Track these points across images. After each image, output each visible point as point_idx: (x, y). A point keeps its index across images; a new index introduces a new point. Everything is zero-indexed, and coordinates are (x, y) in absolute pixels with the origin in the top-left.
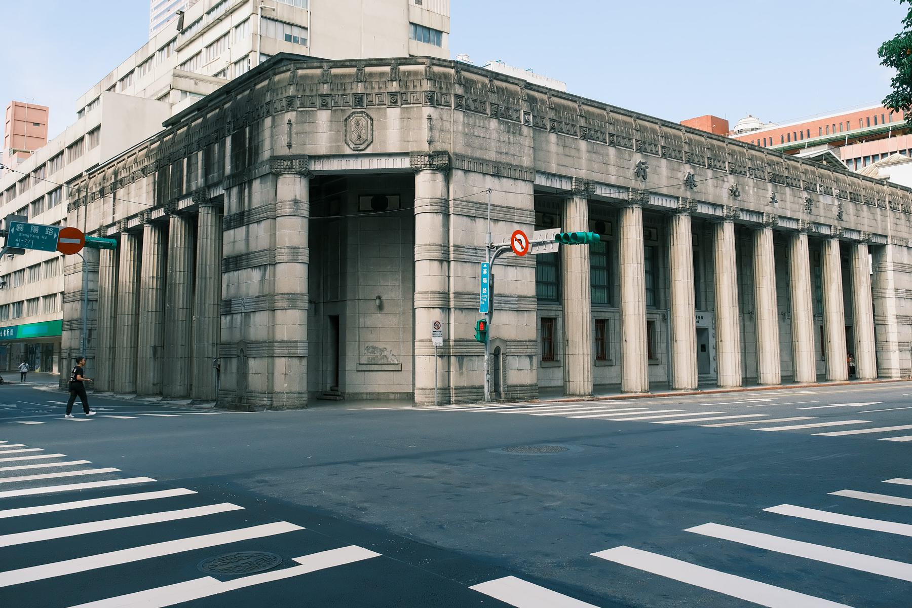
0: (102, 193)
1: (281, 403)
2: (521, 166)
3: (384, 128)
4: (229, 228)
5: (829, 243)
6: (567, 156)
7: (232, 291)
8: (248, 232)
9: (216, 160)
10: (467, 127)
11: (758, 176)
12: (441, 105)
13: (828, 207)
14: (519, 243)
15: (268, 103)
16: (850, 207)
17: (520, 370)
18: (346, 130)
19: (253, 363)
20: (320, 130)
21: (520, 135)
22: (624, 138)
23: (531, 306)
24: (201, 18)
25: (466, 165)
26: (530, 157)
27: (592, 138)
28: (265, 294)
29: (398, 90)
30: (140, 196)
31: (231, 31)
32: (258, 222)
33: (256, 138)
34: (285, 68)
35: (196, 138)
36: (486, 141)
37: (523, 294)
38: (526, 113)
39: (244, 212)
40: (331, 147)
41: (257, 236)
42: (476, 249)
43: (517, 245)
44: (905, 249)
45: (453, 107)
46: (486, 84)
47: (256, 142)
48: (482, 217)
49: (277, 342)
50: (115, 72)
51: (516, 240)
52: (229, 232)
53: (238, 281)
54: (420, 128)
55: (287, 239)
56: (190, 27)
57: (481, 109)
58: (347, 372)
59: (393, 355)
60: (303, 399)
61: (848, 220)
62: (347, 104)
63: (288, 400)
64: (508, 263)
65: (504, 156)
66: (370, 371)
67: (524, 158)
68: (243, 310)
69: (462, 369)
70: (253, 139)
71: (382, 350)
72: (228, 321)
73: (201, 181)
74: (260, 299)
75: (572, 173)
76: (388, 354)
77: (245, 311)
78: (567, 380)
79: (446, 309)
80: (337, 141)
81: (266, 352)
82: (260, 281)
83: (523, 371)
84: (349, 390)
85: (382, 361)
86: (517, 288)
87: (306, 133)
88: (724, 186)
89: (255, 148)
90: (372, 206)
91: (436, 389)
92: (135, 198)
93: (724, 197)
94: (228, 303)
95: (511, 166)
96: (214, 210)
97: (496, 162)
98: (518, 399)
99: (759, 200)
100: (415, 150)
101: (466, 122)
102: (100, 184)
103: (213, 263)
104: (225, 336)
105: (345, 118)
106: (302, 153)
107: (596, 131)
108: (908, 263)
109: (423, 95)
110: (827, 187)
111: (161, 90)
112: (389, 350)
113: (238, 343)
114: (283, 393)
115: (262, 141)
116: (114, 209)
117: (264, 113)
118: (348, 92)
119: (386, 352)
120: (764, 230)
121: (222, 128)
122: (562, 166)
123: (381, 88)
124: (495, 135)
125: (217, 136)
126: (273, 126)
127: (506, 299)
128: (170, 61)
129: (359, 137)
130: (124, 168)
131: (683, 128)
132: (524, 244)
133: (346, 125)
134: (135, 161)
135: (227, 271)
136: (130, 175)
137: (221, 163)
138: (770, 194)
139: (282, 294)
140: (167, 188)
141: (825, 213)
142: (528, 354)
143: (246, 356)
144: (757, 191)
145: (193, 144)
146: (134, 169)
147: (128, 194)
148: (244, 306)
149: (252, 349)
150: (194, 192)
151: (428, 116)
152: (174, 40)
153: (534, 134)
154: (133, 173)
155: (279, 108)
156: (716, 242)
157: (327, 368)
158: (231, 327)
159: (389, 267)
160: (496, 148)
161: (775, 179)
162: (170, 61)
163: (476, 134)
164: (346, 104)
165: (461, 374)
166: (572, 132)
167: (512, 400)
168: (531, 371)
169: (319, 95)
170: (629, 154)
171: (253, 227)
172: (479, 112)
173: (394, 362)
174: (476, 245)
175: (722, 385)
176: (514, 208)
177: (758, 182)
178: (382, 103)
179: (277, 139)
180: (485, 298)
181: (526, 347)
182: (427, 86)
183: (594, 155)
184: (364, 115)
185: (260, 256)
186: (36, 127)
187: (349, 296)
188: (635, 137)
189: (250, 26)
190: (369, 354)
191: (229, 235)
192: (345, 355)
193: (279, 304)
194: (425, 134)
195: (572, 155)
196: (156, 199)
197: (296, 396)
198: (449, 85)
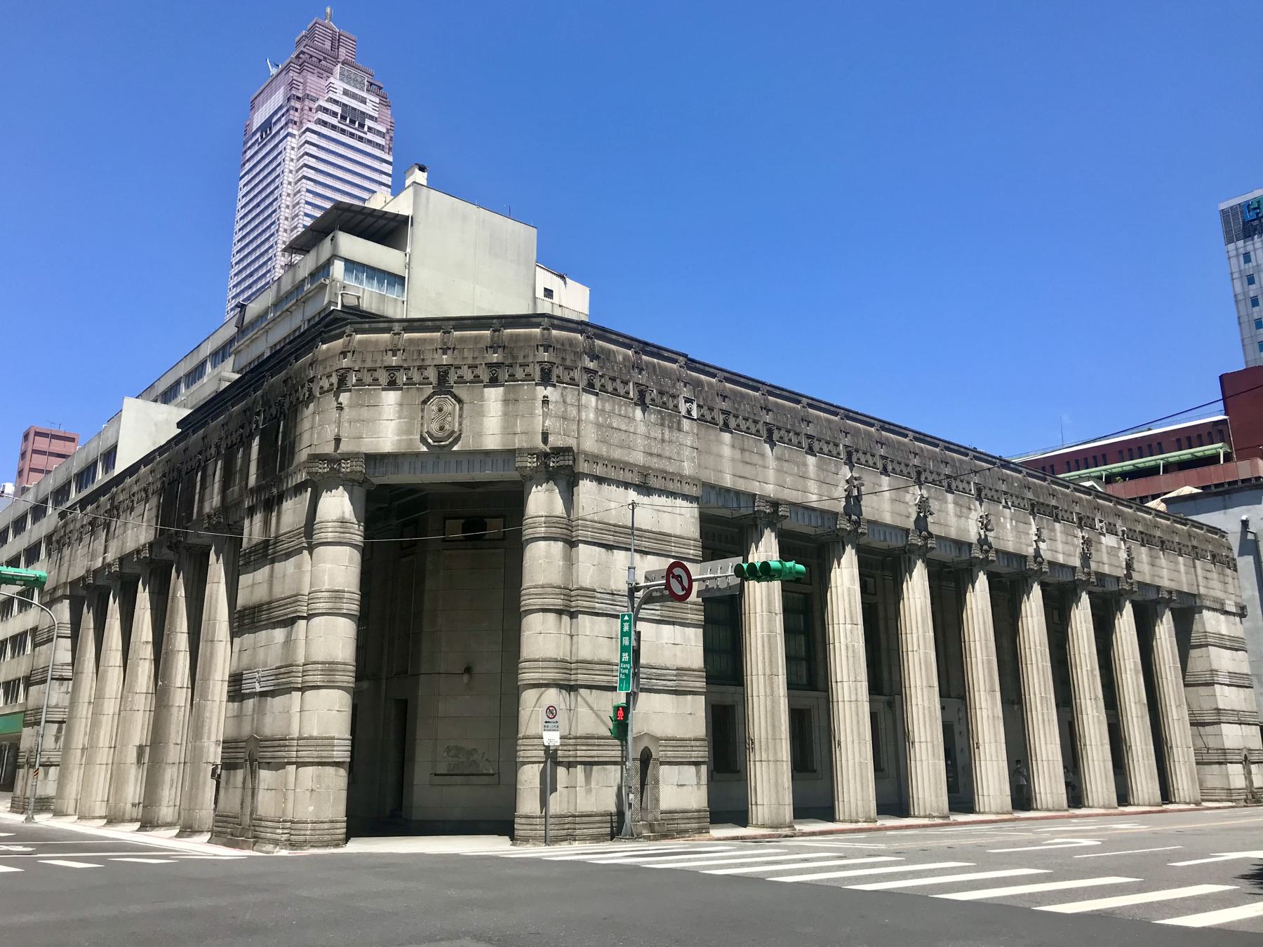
2: (681, 476)
6: (747, 463)
8: (272, 571)
9: (238, 468)
10: (601, 415)
11: (1016, 504)
12: (563, 383)
13: (1113, 551)
15: (311, 380)
16: (1143, 554)
17: (681, 785)
20: (385, 417)
21: (679, 429)
22: (828, 443)
25: (599, 470)
29: (501, 360)
33: (293, 430)
36: (629, 437)
37: (685, 665)
40: (400, 441)
41: (284, 575)
42: (613, 594)
43: (675, 585)
46: (629, 356)
54: (532, 414)
55: (326, 578)
57: (622, 391)
58: (415, 787)
59: (487, 760)
60: (338, 831)
61: (1141, 570)
62: (426, 381)
63: (313, 832)
64: (661, 616)
65: (655, 460)
67: (685, 464)
69: (590, 784)
71: (471, 752)
73: (216, 500)
75: (755, 488)
80: (409, 431)
83: (685, 787)
86: (675, 655)
87: (364, 421)
88: (970, 516)
93: (972, 531)
94: (238, 677)
95: (666, 475)
97: (644, 467)
98: (678, 833)
99: (1020, 538)
100: (525, 445)
101: (600, 407)
105: (422, 399)
106: (356, 450)
107: (788, 432)
108: (1227, 634)
109: (538, 369)
110: (1110, 524)
114: (306, 822)
115: (300, 434)
117: (304, 395)
118: (427, 363)
122: (740, 477)
123: (477, 357)
124: (642, 429)
127: (659, 671)
129: (442, 428)
131: (911, 433)
132: (686, 584)
137: (245, 471)
138: (1034, 530)
141: (1109, 558)
144: (1016, 525)
153: (698, 429)
155: (326, 386)
160: (644, 447)
161: (1036, 509)
163: (615, 425)
166: (753, 430)
167: (670, 835)
168: (699, 789)
169: (385, 367)
172: (620, 396)
174: (613, 588)
176: (670, 535)
177: (1017, 513)
178: (477, 379)
180: (626, 668)
181: (690, 749)
183: (786, 464)
186: (21, 437)
187: (424, 668)
188: (843, 441)
192: (412, 759)
195: (755, 462)
197: (326, 826)
198: (578, 355)
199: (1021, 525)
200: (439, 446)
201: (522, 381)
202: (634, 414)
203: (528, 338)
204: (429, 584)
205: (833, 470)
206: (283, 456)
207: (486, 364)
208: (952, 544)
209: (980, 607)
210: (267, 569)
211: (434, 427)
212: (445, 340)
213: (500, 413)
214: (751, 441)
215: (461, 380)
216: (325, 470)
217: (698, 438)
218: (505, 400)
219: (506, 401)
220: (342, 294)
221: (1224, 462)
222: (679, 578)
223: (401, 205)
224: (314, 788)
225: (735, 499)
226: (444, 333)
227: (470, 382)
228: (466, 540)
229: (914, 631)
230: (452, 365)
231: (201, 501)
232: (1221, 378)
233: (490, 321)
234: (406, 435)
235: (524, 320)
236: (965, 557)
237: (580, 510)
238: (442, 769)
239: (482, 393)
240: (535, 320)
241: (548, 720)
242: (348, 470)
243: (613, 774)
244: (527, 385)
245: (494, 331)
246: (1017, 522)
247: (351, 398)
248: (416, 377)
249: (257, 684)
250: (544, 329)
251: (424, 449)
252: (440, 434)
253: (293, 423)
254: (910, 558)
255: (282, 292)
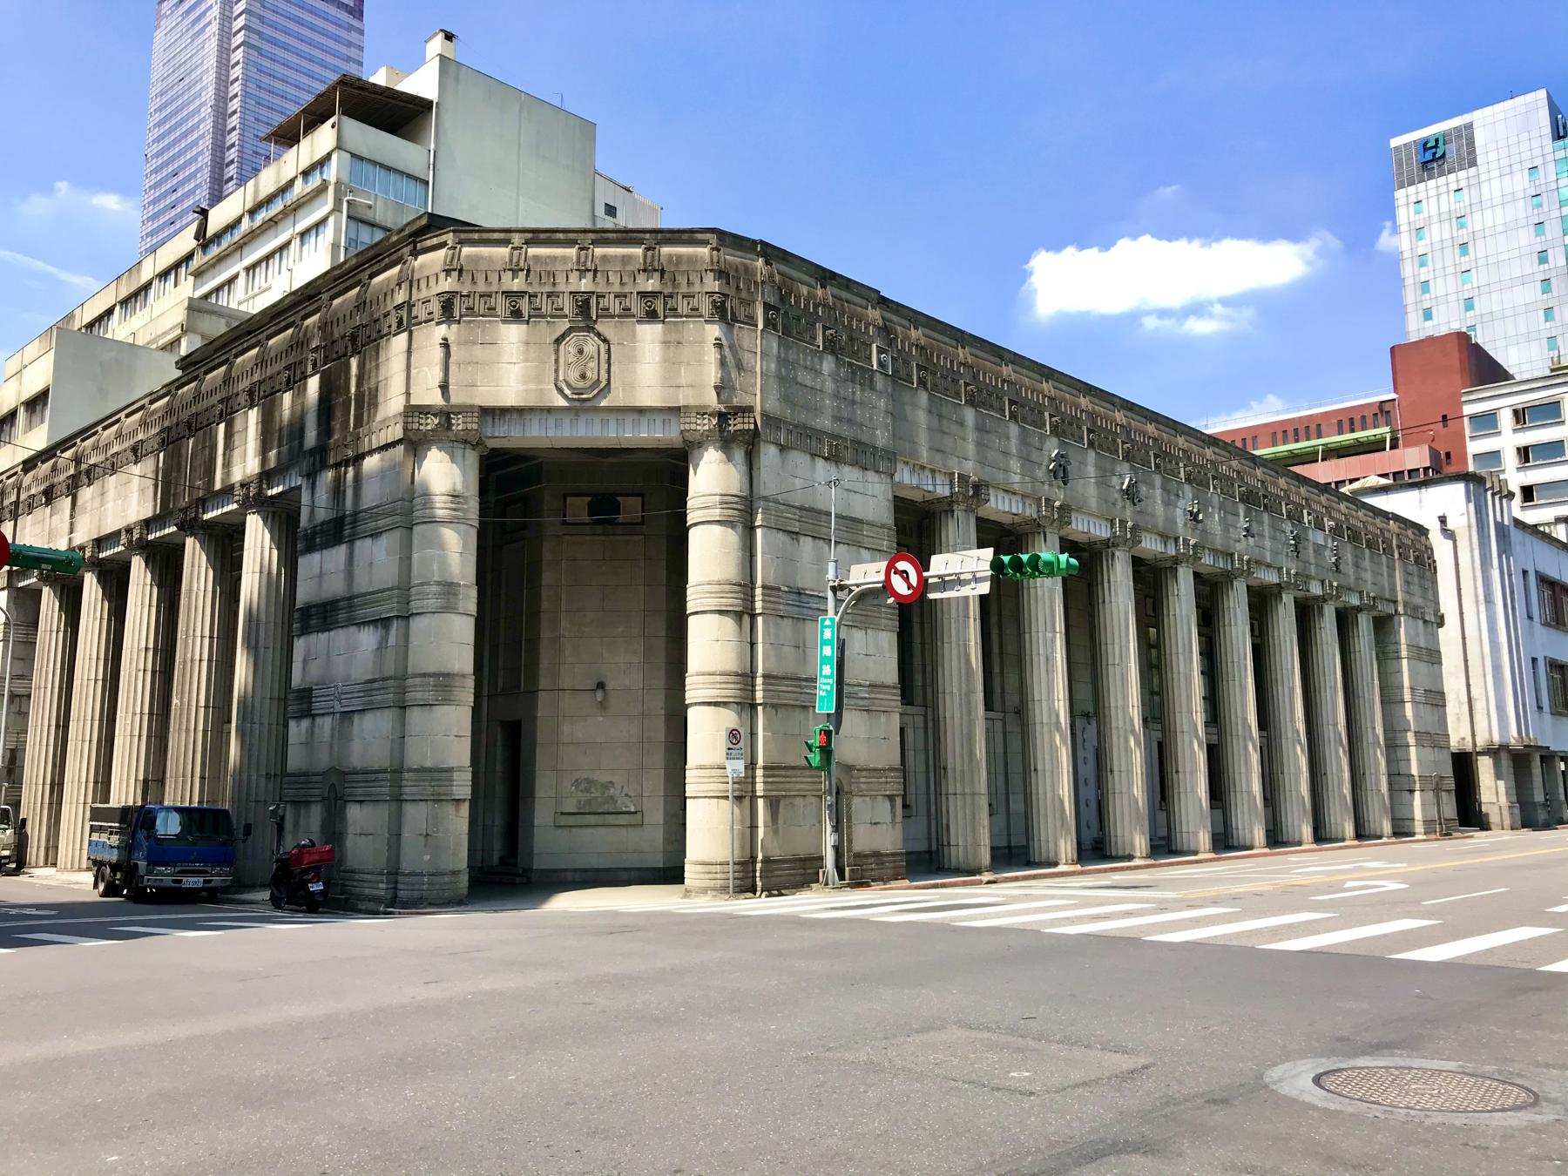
0: (49, 495)
1: (416, 894)
3: (633, 359)
4: (310, 549)
5: (1321, 609)
7: (315, 672)
14: (903, 577)
17: (876, 824)
18: (557, 361)
19: (355, 813)
20: (506, 358)
21: (872, 388)
23: (893, 703)
24: (239, 221)
26: (888, 431)
27: (983, 404)
28: (386, 675)
29: (657, 289)
30: (126, 496)
31: (293, 242)
32: (375, 535)
33: (373, 374)
34: (435, 241)
35: (245, 384)
38: (880, 351)
39: (344, 517)
44: (1420, 623)
45: (761, 326)
47: (373, 381)
48: (810, 533)
49: (411, 770)
50: (78, 312)
51: (895, 573)
52: (309, 556)
53: (328, 651)
54: (700, 361)
56: (218, 236)
59: (626, 795)
66: (581, 826)
67: (878, 432)
68: (338, 708)
70: (366, 377)
72: (303, 731)
74: (375, 685)
76: (617, 793)
77: (342, 710)
78: (945, 843)
79: (747, 706)
80: (539, 380)
81: (386, 790)
82: (377, 649)
84: (538, 864)
85: (606, 808)
86: (867, 668)
89: (370, 393)
90: (619, 503)
91: (731, 863)
92: (115, 501)
96: (277, 518)
99: (1228, 531)
100: (691, 402)
102: (46, 478)
103: (272, 619)
104: (295, 761)
105: (555, 336)
106: (469, 401)
111: (165, 334)
112: (618, 786)
113: (323, 774)
114: (421, 874)
115: (386, 379)
116: (72, 524)
117: (390, 326)
118: (560, 288)
119: (612, 790)
120: (1235, 583)
121: (301, 363)
123: (625, 284)
124: (829, 386)
125: (289, 376)
126: (229, 436)
128: (187, 288)
129: (583, 376)
130: (95, 448)
133: (557, 352)
134: (119, 435)
135: (305, 631)
136: (107, 459)
139: (424, 675)
140: (183, 476)
141: (1315, 557)
142: (888, 793)
143: (341, 798)
145: (237, 395)
146: (116, 449)
147: (102, 494)
148: (340, 700)
149: (354, 785)
150: (237, 485)
151: (716, 339)
152: (189, 257)
154: (113, 456)
155: (423, 316)
156: (1165, 600)
157: (493, 822)
158: (310, 741)
159: (620, 630)
162: (187, 288)
164: (559, 313)
165: (776, 832)
168: (893, 827)
170: (1040, 439)
171: (363, 546)
173: (627, 809)
174: (800, 586)
175: (1179, 848)
177: (1226, 502)
178: (626, 313)
179: (418, 373)
180: (828, 684)
182: (711, 284)
184: (592, 335)
185: (377, 602)
187: (544, 682)
189: (328, 234)
190: (579, 794)
191: (309, 564)
192: (532, 795)
193: (413, 696)
194: (712, 374)
196: (159, 501)
199: (1230, 517)
200: (578, 400)
201: (686, 316)
202: (821, 366)
203: (692, 260)
204: (547, 577)
205: (1037, 445)
206: (359, 406)
207: (638, 293)
208: (1157, 537)
209: (1184, 612)
210: (342, 550)
211: (573, 376)
212: (582, 260)
213: (657, 359)
214: (950, 405)
215: (606, 313)
216: (706, 428)
217: (893, 400)
218: (665, 342)
219: (666, 343)
220: (348, 201)
221: (1391, 448)
222: (904, 575)
223: (422, 83)
224: (429, 832)
225: (930, 477)
226: (581, 249)
227: (619, 316)
228: (593, 524)
229: (1116, 641)
230: (593, 293)
231: (227, 465)
232: (1392, 349)
233: (642, 235)
234: (525, 383)
235: (686, 236)
236: (1171, 551)
237: (762, 488)
238: (570, 806)
239: (634, 332)
240: (699, 236)
241: (732, 746)
242: (460, 428)
243: (802, 809)
244: (694, 322)
245: (581, 249)
246: (1225, 513)
247: (459, 330)
248: (546, 307)
249: (336, 703)
250: (713, 249)
251: (565, 404)
252: (581, 384)
253: (373, 364)
254: (1113, 554)
255: (263, 194)
